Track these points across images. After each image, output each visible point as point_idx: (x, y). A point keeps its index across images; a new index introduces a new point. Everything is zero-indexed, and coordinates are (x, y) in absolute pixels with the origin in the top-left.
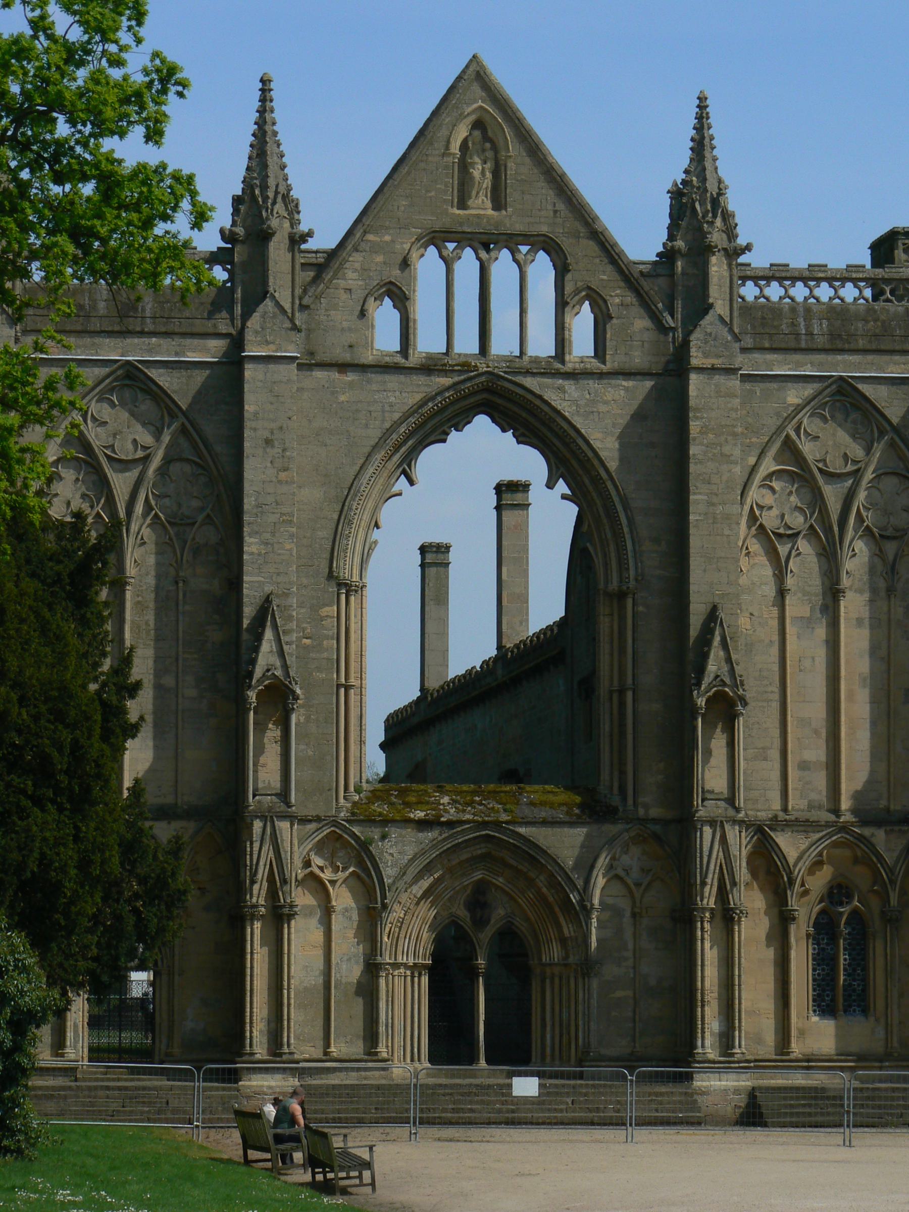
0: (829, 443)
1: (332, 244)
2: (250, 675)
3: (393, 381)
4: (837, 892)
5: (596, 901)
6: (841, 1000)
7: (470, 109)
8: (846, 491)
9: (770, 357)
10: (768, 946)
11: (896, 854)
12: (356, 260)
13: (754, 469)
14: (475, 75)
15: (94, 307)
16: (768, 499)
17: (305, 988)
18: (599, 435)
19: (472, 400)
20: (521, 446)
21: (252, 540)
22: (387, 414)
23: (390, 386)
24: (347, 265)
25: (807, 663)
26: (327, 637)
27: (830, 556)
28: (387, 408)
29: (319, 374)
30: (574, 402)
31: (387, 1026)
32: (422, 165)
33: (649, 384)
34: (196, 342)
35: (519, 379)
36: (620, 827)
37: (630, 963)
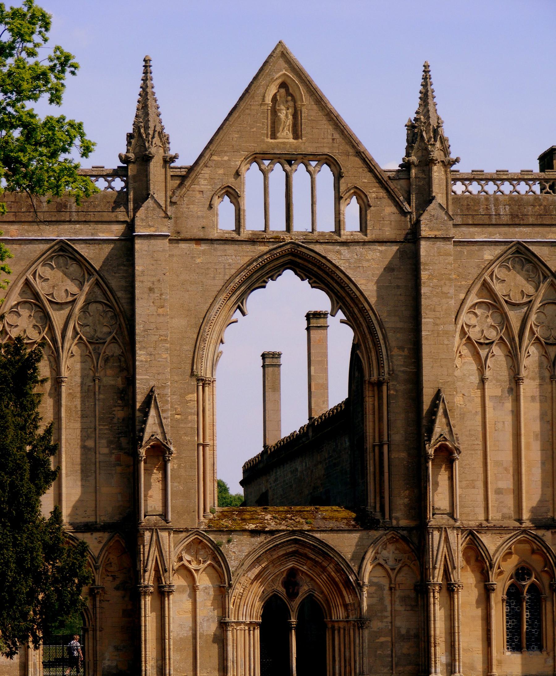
1: (191, 163)
2: (141, 439)
3: (230, 249)
4: (521, 572)
5: (366, 580)
7: (277, 76)
8: (523, 315)
10: (477, 607)
14: (281, 54)
16: (473, 321)
18: (363, 282)
19: (282, 260)
21: (142, 352)
22: (227, 271)
23: (229, 252)
24: (200, 176)
25: (500, 426)
26: (191, 414)
27: (513, 357)
28: (227, 267)
31: (233, 662)
32: (248, 111)
33: (395, 248)
34: (105, 226)
35: (311, 246)
36: (381, 532)
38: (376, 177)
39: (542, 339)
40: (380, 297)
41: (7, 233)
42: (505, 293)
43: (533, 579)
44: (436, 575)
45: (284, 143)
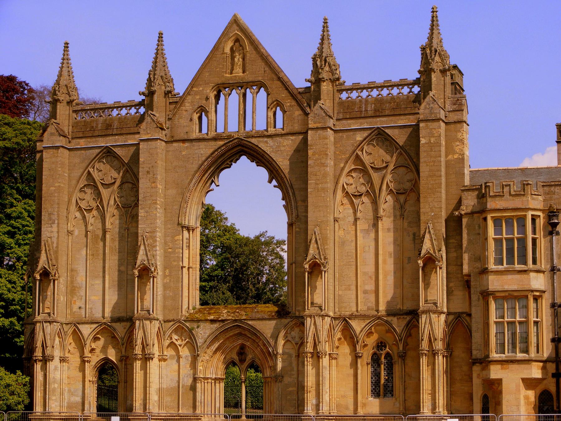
0: (374, 155)
3: (202, 144)
4: (380, 345)
5: (280, 351)
6: (382, 391)
7: (232, 35)
8: (383, 175)
9: (349, 121)
10: (351, 368)
11: (402, 328)
12: (189, 98)
13: (343, 169)
14: (235, 21)
15: (97, 127)
16: (351, 181)
17: (171, 388)
18: (281, 160)
19: (235, 150)
20: (259, 167)
23: (201, 147)
24: (186, 101)
25: (367, 249)
27: (375, 203)
28: (200, 156)
29: (175, 144)
30: (271, 147)
31: (201, 403)
32: (214, 59)
34: (131, 136)
35: (249, 140)
36: (289, 320)
37: (295, 376)
38: (290, 93)
39: (394, 190)
40: (291, 169)
41: (79, 144)
42: (372, 162)
43: (387, 349)
44: (308, 346)
45: (235, 76)
